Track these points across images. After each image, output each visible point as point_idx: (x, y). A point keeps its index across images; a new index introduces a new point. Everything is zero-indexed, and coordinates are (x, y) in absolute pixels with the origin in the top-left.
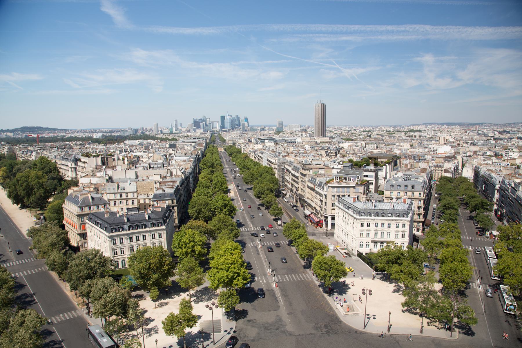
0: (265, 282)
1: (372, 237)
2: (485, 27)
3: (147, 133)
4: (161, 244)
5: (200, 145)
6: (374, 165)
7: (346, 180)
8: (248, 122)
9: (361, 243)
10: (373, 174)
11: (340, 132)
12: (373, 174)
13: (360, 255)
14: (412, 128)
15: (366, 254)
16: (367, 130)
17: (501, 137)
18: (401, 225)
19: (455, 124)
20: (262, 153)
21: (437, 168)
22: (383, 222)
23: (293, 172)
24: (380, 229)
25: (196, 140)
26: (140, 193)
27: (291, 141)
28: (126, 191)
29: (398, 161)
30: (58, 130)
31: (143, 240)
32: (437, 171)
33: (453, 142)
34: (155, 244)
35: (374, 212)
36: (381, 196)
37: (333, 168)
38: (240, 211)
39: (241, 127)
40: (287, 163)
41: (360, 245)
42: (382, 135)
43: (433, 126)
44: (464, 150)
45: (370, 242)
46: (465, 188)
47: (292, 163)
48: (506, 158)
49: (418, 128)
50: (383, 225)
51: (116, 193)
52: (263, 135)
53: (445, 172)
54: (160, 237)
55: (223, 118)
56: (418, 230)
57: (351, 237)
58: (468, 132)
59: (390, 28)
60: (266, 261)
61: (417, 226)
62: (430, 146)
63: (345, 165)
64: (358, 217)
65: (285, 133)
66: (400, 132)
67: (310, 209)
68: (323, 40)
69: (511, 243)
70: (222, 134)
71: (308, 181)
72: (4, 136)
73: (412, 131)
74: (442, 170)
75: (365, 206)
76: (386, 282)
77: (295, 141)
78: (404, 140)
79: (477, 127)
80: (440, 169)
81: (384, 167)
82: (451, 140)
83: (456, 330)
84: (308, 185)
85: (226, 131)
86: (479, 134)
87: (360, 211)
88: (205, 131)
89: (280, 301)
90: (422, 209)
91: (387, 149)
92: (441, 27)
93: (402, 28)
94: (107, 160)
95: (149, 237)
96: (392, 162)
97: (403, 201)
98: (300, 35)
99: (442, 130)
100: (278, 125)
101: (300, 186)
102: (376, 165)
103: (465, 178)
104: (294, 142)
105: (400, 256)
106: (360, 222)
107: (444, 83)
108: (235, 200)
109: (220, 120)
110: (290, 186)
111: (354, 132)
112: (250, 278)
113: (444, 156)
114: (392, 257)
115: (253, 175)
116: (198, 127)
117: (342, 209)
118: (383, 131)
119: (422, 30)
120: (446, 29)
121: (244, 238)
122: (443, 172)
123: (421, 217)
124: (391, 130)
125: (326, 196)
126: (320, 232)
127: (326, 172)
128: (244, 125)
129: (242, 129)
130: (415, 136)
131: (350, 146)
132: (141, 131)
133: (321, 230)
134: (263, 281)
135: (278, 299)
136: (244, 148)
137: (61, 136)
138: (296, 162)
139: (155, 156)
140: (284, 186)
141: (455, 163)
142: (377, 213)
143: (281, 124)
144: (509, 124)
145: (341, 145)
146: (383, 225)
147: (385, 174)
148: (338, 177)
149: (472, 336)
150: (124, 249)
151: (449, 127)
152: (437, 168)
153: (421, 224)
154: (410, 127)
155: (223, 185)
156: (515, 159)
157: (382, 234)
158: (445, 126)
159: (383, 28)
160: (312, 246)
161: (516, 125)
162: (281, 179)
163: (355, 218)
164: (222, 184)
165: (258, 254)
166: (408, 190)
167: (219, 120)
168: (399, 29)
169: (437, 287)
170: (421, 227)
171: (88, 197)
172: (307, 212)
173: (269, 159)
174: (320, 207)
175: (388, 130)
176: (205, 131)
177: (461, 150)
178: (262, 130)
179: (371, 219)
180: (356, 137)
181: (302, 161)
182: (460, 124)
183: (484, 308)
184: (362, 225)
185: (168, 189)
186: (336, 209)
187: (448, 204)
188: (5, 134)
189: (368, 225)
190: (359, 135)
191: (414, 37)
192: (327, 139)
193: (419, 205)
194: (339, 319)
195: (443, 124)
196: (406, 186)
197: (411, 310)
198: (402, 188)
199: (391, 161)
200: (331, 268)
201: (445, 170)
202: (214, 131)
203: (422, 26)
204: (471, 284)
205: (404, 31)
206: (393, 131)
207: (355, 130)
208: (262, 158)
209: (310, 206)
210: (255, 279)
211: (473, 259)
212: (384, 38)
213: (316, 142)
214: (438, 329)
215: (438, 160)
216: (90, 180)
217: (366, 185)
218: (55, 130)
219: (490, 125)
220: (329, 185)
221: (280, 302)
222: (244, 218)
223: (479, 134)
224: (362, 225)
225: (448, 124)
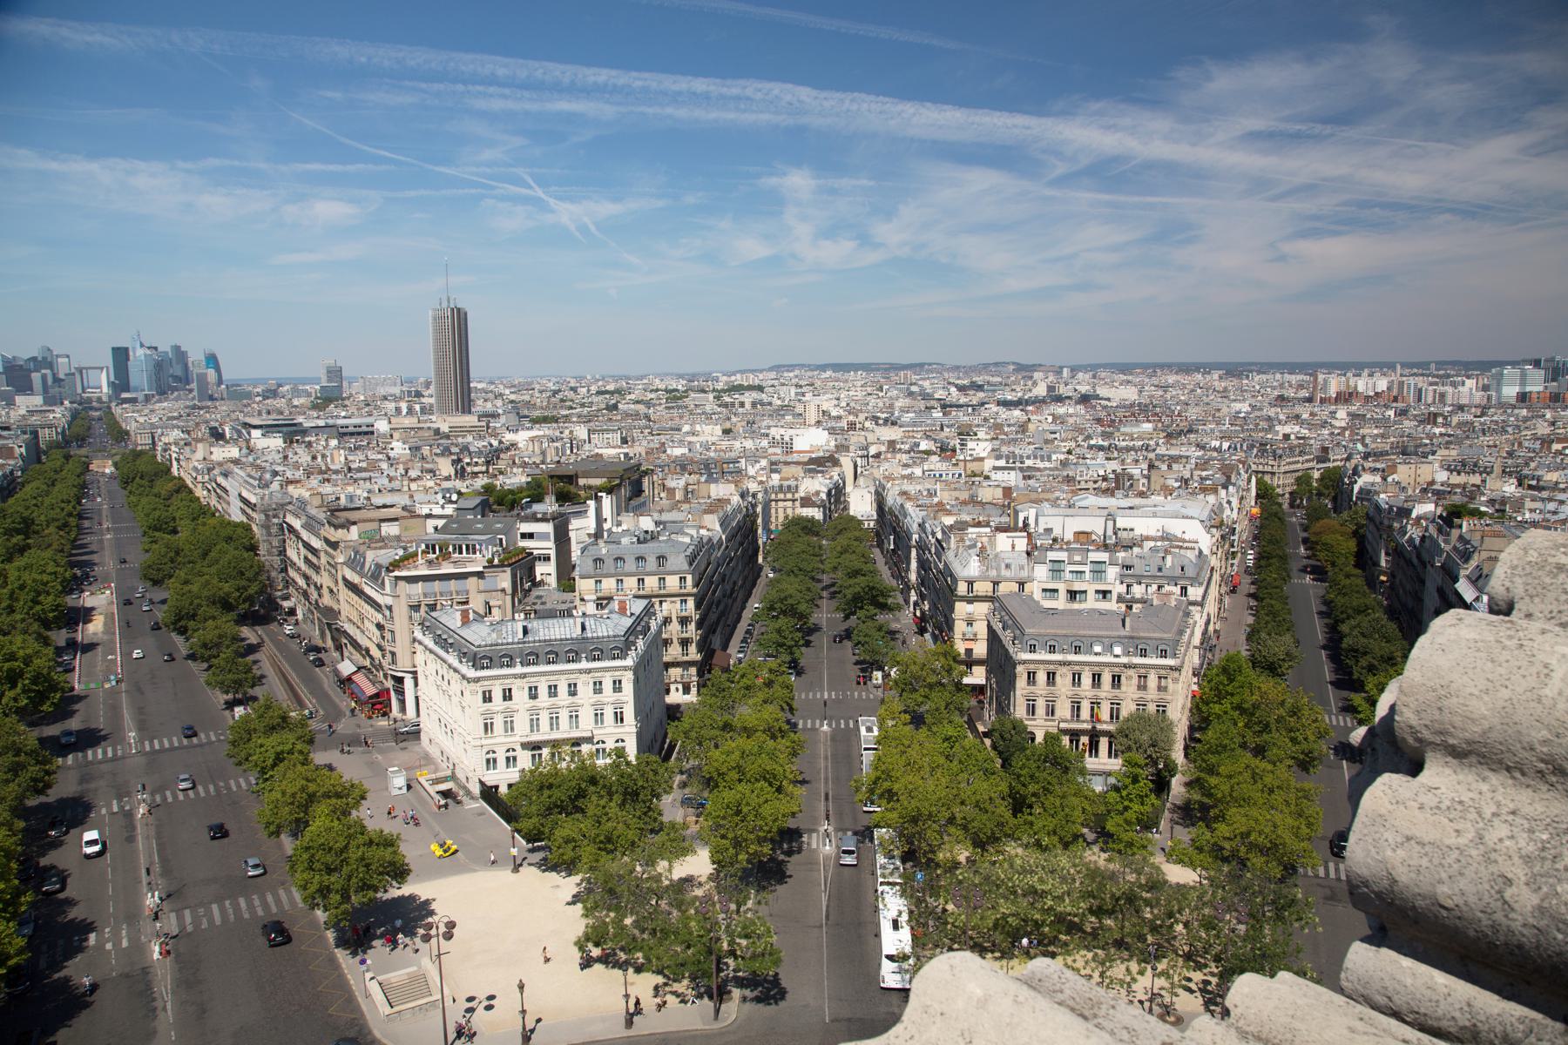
0: (125, 943)
1: (522, 732)
2: (946, 107)
6: (557, 501)
7: (461, 553)
8: (218, 370)
9: (491, 756)
10: (548, 528)
11: (527, 398)
12: (548, 528)
13: (489, 794)
14: (738, 379)
15: (510, 786)
16: (611, 387)
17: (963, 400)
18: (608, 686)
19: (855, 367)
20: (226, 475)
21: (781, 496)
22: (553, 680)
23: (305, 535)
24: (546, 705)
27: (345, 430)
29: (646, 482)
32: (781, 504)
33: (840, 418)
35: (521, 650)
36: (568, 596)
37: (429, 516)
38: (107, 686)
40: (290, 507)
41: (488, 761)
42: (648, 404)
43: (797, 372)
44: (862, 440)
45: (518, 748)
46: (839, 549)
47: (303, 504)
48: (962, 457)
49: (752, 380)
50: (553, 691)
52: (269, 413)
53: (802, 506)
55: (121, 355)
56: (687, 690)
57: (461, 739)
58: (885, 387)
59: (700, 85)
61: (682, 676)
62: (773, 431)
63: (464, 504)
64: (472, 673)
65: (347, 402)
66: (704, 391)
67: (357, 656)
68: (497, 105)
69: (921, 699)
70: (117, 410)
71: (343, 563)
73: (739, 389)
74: (794, 501)
75: (494, 635)
76: (554, 874)
77: (370, 429)
78: (709, 417)
79: (906, 375)
80: (789, 496)
81: (592, 504)
82: (834, 413)
83: (736, 993)
84: (344, 579)
85: (133, 401)
86: (911, 394)
87: (475, 654)
88: (52, 400)
89: (165, 1008)
90: (692, 627)
91: (652, 445)
92: (838, 95)
93: (734, 88)
96: (619, 486)
97: (617, 608)
98: (424, 86)
99: (818, 383)
100: (324, 378)
101: (324, 580)
102: (562, 498)
103: (853, 518)
104: (366, 433)
105: (583, 786)
106: (479, 688)
107: (836, 252)
108: (100, 649)
109: (109, 361)
110: (301, 582)
111: (571, 395)
112: (20, 952)
113: (806, 460)
114: (558, 794)
115: (177, 553)
116: (26, 388)
117: (431, 651)
118: (657, 390)
119: (788, 98)
120: (852, 101)
121: (92, 786)
122: (798, 504)
123: (693, 649)
124: (680, 387)
125: (390, 608)
126: (382, 729)
127: (406, 529)
128: (202, 379)
129: (195, 393)
130: (742, 405)
131: (532, 439)
133: (383, 723)
134: (117, 944)
135: (159, 1004)
136: (178, 460)
138: (317, 501)
140: (289, 583)
141: (831, 478)
142: (530, 654)
143: (335, 373)
144: (986, 366)
145: (509, 437)
146: (553, 691)
147: (593, 525)
148: (460, 548)
149: (776, 1003)
151: (839, 375)
152: (781, 496)
153: (693, 670)
154: (733, 378)
155: (41, 598)
156: (982, 459)
157: (554, 721)
158: (829, 373)
159: (683, 84)
160: (303, 789)
161: (1000, 369)
162: (277, 560)
163: (464, 677)
164: (39, 594)
165: (131, 839)
166: (648, 569)
167: (108, 361)
168: (725, 89)
169: (698, 864)
170: (695, 679)
172: (346, 668)
173: (245, 494)
174: (379, 647)
175: (670, 387)
176: (52, 400)
177: (856, 439)
178: (272, 393)
179: (515, 676)
180: (567, 412)
181: (338, 499)
182: (867, 367)
183: (828, 906)
184: (487, 698)
186: (419, 648)
187: (782, 600)
189: (508, 695)
190: (583, 405)
191: (765, 117)
192: (470, 420)
193: (684, 614)
194: (370, 1032)
195: (823, 368)
196: (640, 558)
197: (615, 954)
198: (631, 565)
199: (617, 482)
200: (344, 860)
201: (802, 498)
202: (90, 400)
203: (790, 86)
204: (805, 838)
205: (738, 98)
206: (686, 391)
207: (574, 389)
208: (226, 491)
209: (356, 645)
210: (87, 939)
211: (826, 758)
212: (682, 113)
213: (437, 431)
214: (682, 1002)
215: (788, 471)
217: (523, 566)
219: (940, 369)
220: (397, 573)
221: (161, 1015)
222: (115, 710)
223: (911, 394)
224: (487, 698)
225: (837, 367)
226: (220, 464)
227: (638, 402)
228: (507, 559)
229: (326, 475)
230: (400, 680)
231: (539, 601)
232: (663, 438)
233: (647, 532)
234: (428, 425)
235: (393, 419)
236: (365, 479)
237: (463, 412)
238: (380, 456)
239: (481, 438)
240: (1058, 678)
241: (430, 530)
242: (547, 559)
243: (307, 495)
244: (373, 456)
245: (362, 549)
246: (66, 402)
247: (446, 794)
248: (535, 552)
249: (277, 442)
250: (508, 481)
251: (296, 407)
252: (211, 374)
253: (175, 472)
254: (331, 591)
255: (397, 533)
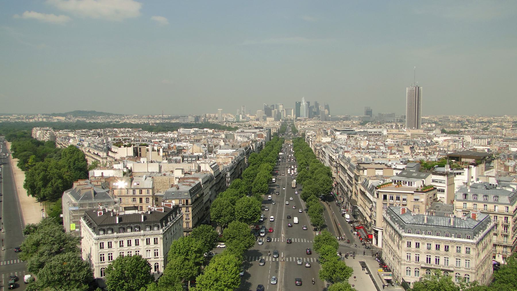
3: (210, 120)
4: (122, 254)
5: (261, 136)
23: (349, 172)
25: (257, 130)
26: (160, 190)
27: (370, 133)
28: (141, 186)
30: (112, 114)
31: (128, 246)
34: (123, 253)
37: (395, 169)
39: (320, 116)
45: (420, 268)
51: (129, 189)
54: (156, 242)
60: (281, 282)
72: (56, 121)
75: (414, 220)
81: (466, 170)
84: (360, 190)
94: (140, 151)
95: (115, 245)
104: (378, 135)
129: (321, 118)
131: (445, 140)
132: (203, 118)
137: (116, 121)
139: (194, 148)
150: (113, 255)
171: (91, 191)
185: (184, 186)
188: (57, 118)
192: (421, 132)
216: (102, 173)
218: (109, 114)
226: (324, 143)
227: (498, 127)
228: (424, 189)
229: (359, 149)
230: (377, 232)
231: (437, 209)
232: (508, 143)
233: (490, 184)
234: (402, 133)
235: (389, 130)
236: (373, 153)
237: (417, 128)
238: (382, 144)
239: (423, 139)
240: (450, 248)
241: (395, 174)
242: (443, 191)
243: (350, 157)
244: (379, 143)
245: (368, 179)
246: (281, 120)
247: (388, 281)
248: (438, 188)
249: (345, 137)
250: (432, 157)
251: (354, 124)
252: (326, 111)
253: (310, 147)
254: (355, 194)
255: (382, 174)
